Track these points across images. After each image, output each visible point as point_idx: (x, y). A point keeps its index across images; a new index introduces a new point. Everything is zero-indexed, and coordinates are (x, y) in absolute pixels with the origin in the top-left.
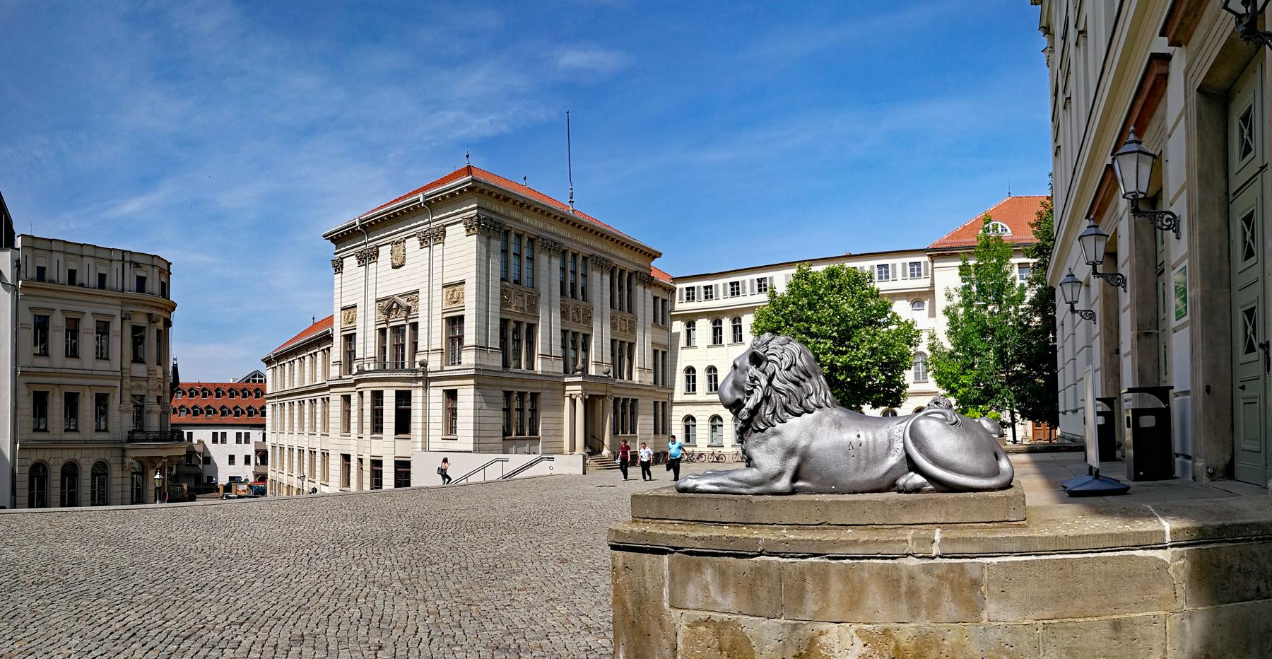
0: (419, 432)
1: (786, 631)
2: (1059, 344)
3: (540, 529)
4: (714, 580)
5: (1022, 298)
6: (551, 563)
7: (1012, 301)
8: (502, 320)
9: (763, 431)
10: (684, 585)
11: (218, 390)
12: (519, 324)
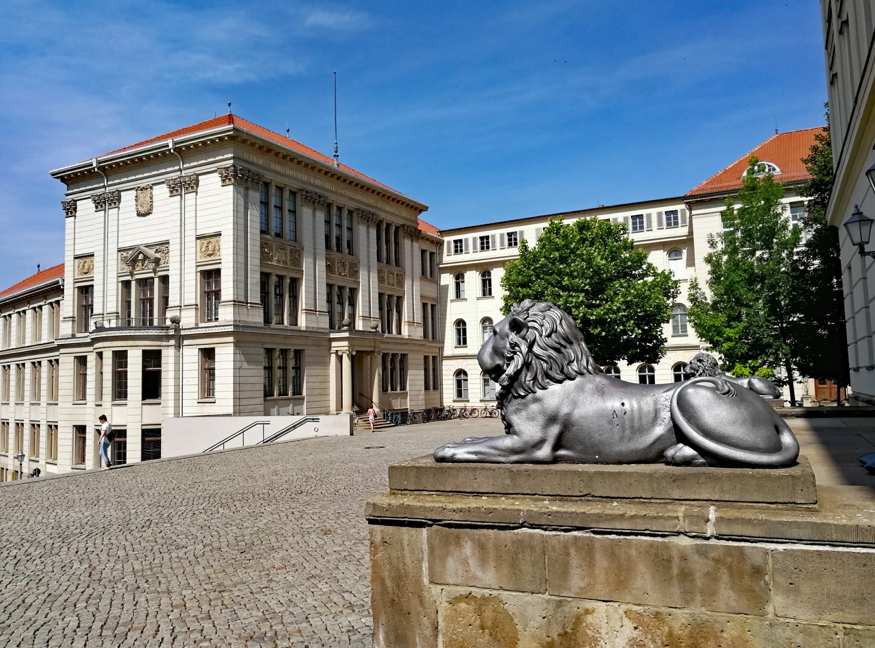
0: (171, 396)
1: (551, 608)
2: (846, 289)
3: (303, 498)
4: (473, 554)
5: (796, 240)
6: (313, 535)
7: (784, 245)
8: (262, 273)
9: (523, 397)
10: (443, 559)
12: (281, 278)
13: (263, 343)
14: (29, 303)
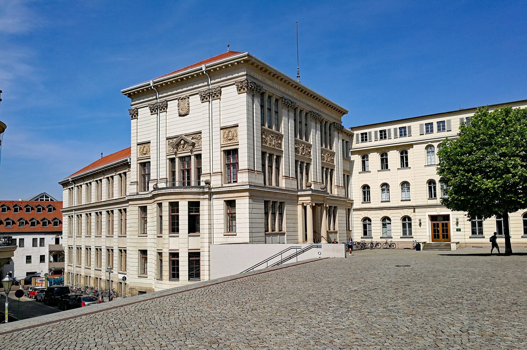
0: (207, 231)
11: (16, 207)
13: (264, 197)
14: (104, 175)
